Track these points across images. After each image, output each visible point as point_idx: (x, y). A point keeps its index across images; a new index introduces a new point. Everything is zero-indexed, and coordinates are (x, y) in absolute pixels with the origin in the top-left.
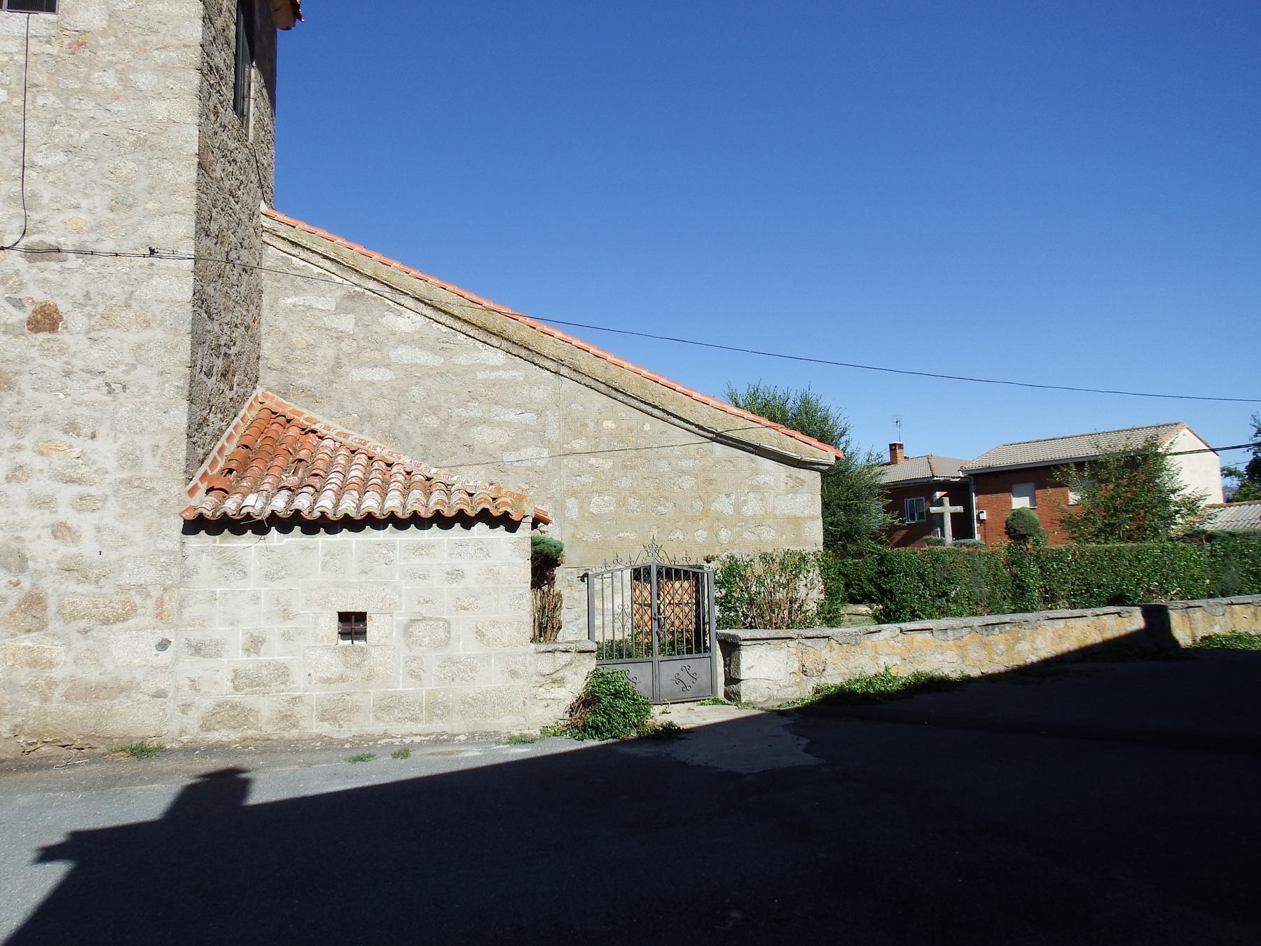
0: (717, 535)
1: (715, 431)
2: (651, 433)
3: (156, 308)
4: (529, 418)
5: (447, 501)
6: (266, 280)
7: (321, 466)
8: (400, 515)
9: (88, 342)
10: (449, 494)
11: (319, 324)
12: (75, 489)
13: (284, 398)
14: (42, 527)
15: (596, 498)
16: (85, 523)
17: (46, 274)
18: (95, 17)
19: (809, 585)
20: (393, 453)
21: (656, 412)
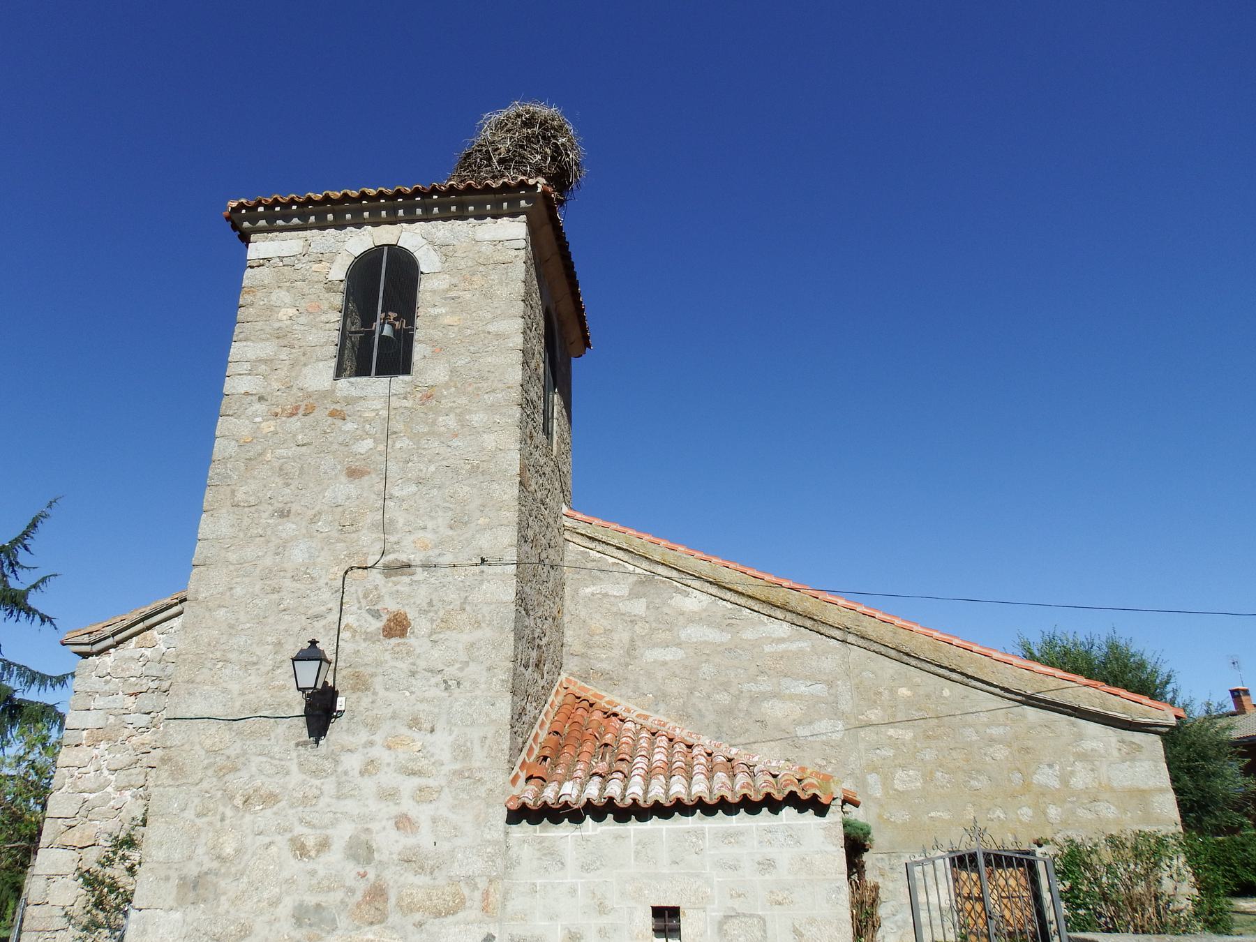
0: (1045, 813)
1: (1024, 693)
2: (951, 699)
3: (486, 609)
4: (820, 689)
5: (752, 784)
6: (568, 574)
7: (627, 750)
8: (707, 800)
9: (430, 644)
10: (753, 775)
11: (615, 609)
12: (416, 781)
13: (586, 682)
14: (387, 819)
15: (900, 773)
16: (422, 814)
17: (399, 587)
18: (440, 374)
19: (1175, 876)
20: (691, 734)
21: (954, 676)
